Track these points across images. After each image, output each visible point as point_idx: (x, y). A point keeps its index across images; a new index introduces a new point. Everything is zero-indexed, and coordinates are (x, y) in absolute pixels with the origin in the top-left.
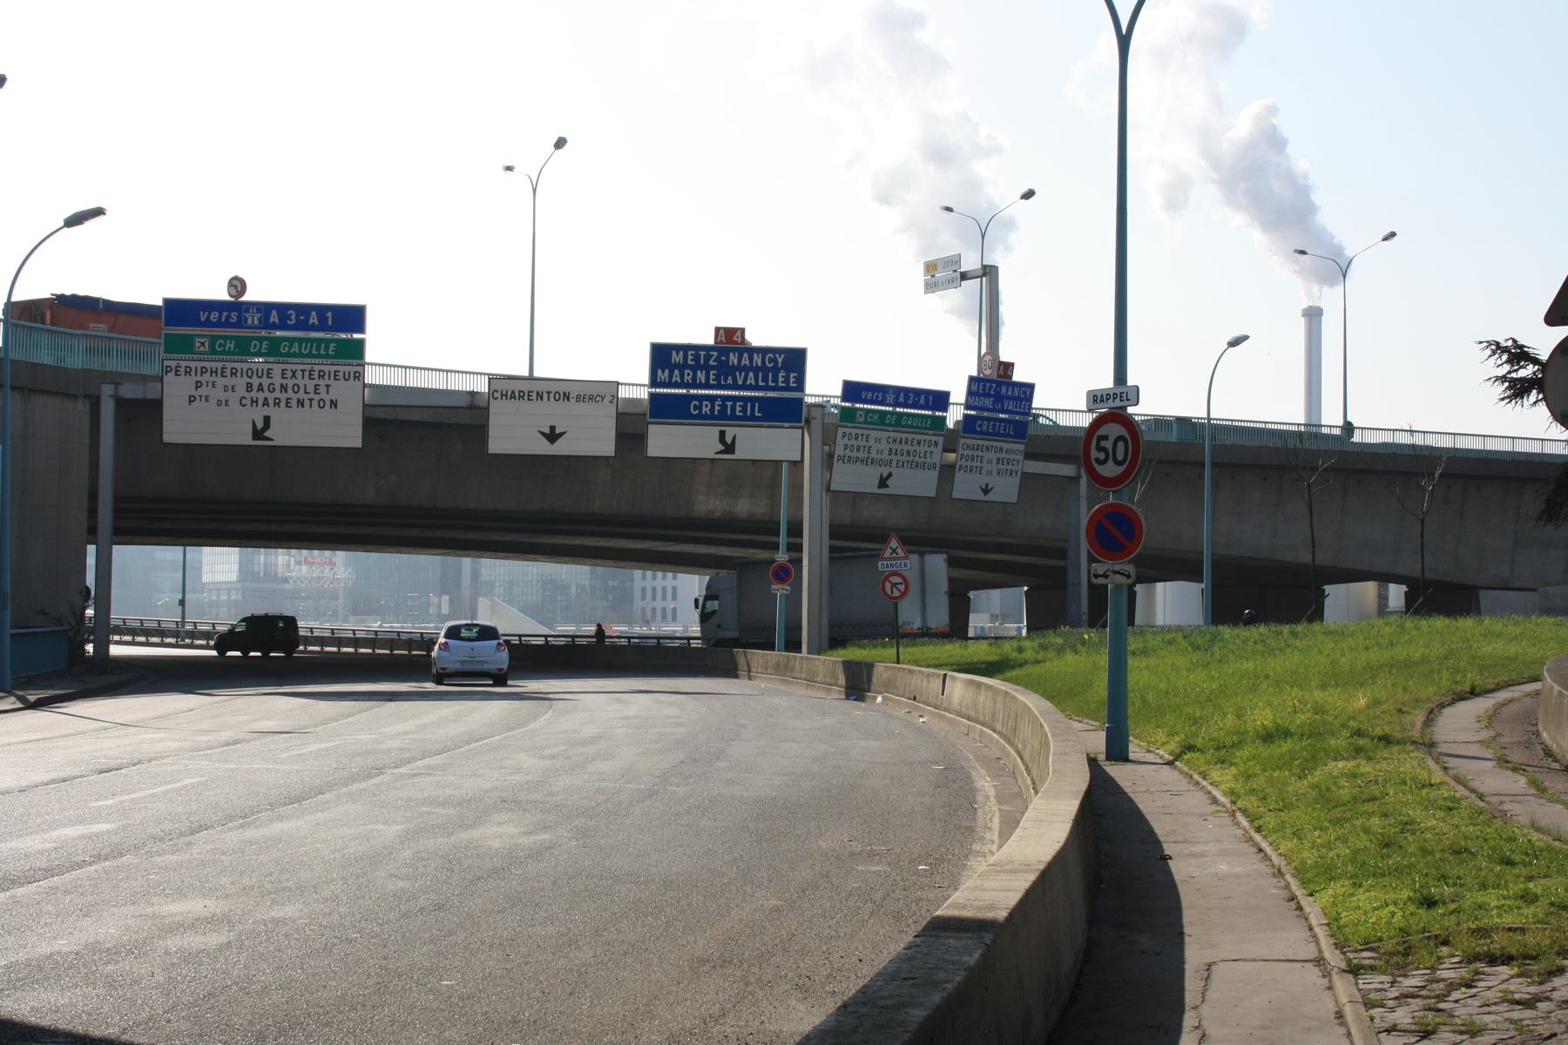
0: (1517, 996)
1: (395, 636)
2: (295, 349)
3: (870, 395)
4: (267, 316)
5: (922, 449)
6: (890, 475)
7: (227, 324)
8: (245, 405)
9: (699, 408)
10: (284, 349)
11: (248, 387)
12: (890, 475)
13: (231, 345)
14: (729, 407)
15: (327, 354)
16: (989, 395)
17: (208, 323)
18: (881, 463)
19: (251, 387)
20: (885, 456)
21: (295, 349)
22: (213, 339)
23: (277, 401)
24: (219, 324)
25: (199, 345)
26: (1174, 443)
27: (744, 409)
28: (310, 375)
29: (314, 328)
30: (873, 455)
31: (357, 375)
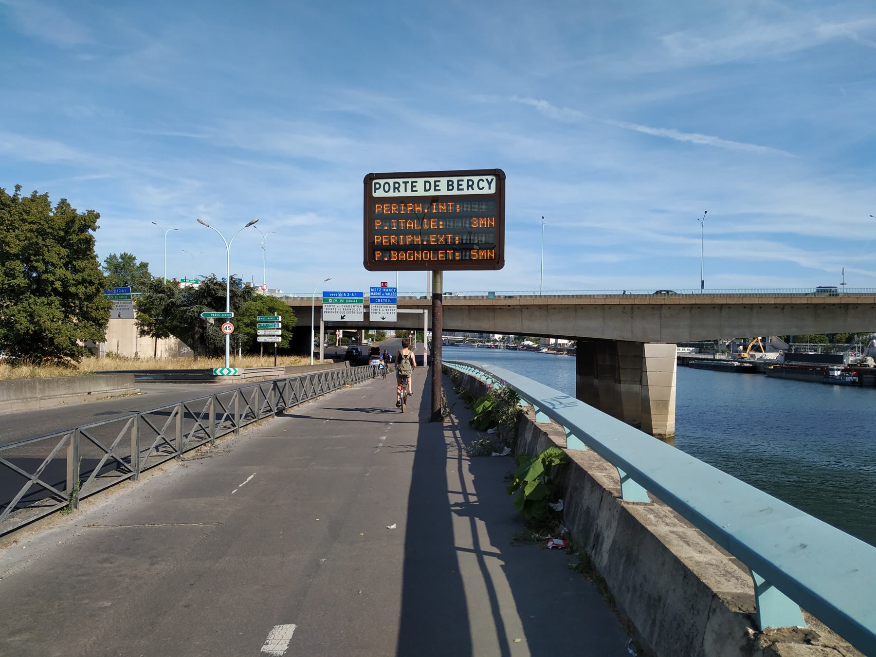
0: (115, 414)
1: (644, 370)
2: (349, 301)
3: (333, 295)
4: (343, 294)
5: (356, 308)
6: (345, 316)
7: (335, 296)
8: (483, 188)
9: (377, 300)
10: (347, 301)
11: (449, 185)
12: (345, 316)
13: (336, 301)
14: (228, 337)
15: (391, 229)
16: (379, 292)
17: (331, 296)
18: (340, 312)
19: (452, 185)
20: (342, 310)
21: (349, 301)
22: (333, 299)
23: (450, 183)
24: (334, 296)
25: (330, 301)
26: (174, 334)
27: (387, 301)
28: (413, 186)
29: (353, 297)
30: (337, 310)
31: (450, 183)
